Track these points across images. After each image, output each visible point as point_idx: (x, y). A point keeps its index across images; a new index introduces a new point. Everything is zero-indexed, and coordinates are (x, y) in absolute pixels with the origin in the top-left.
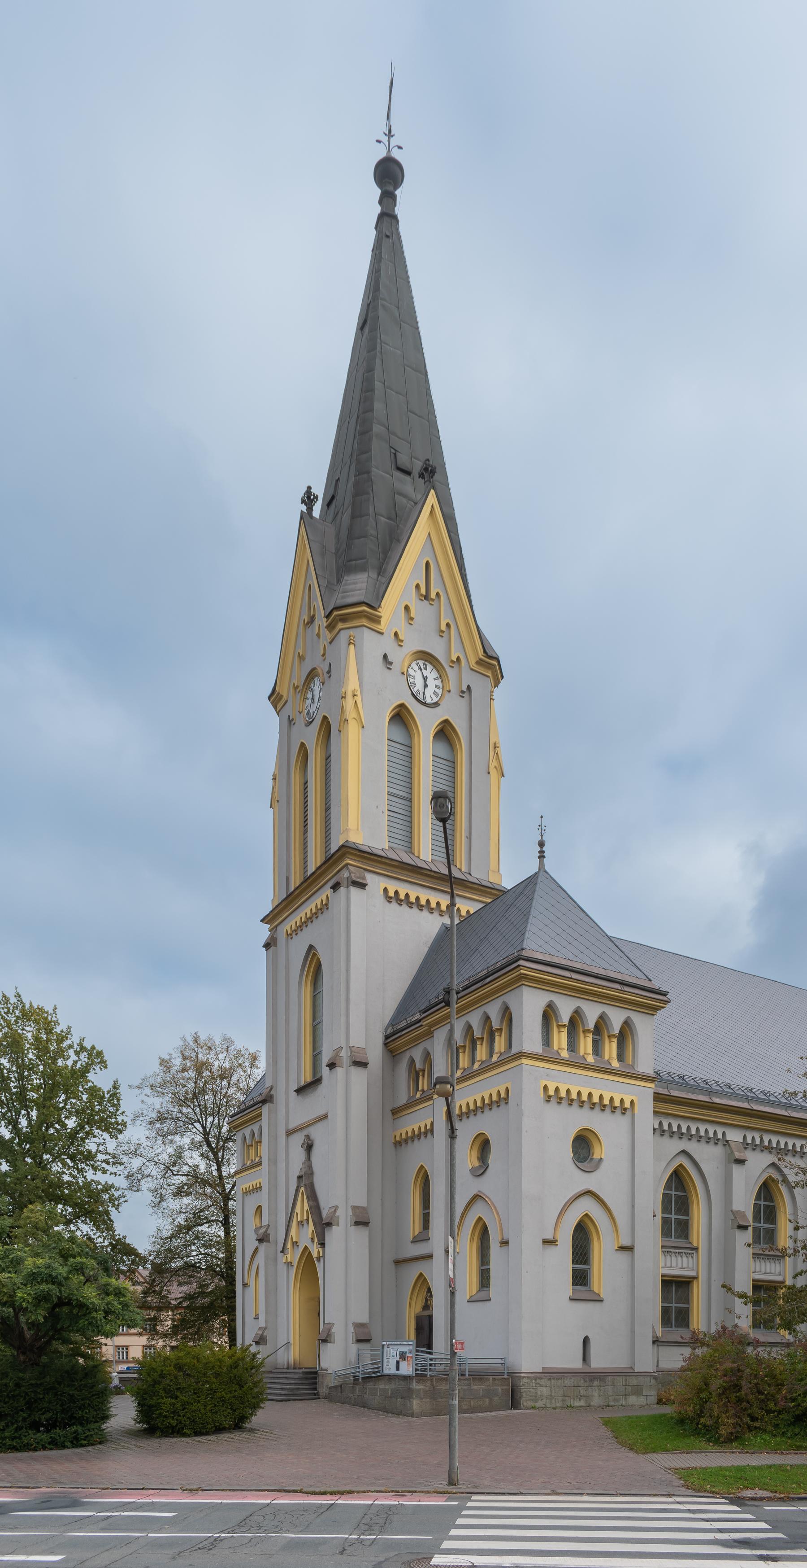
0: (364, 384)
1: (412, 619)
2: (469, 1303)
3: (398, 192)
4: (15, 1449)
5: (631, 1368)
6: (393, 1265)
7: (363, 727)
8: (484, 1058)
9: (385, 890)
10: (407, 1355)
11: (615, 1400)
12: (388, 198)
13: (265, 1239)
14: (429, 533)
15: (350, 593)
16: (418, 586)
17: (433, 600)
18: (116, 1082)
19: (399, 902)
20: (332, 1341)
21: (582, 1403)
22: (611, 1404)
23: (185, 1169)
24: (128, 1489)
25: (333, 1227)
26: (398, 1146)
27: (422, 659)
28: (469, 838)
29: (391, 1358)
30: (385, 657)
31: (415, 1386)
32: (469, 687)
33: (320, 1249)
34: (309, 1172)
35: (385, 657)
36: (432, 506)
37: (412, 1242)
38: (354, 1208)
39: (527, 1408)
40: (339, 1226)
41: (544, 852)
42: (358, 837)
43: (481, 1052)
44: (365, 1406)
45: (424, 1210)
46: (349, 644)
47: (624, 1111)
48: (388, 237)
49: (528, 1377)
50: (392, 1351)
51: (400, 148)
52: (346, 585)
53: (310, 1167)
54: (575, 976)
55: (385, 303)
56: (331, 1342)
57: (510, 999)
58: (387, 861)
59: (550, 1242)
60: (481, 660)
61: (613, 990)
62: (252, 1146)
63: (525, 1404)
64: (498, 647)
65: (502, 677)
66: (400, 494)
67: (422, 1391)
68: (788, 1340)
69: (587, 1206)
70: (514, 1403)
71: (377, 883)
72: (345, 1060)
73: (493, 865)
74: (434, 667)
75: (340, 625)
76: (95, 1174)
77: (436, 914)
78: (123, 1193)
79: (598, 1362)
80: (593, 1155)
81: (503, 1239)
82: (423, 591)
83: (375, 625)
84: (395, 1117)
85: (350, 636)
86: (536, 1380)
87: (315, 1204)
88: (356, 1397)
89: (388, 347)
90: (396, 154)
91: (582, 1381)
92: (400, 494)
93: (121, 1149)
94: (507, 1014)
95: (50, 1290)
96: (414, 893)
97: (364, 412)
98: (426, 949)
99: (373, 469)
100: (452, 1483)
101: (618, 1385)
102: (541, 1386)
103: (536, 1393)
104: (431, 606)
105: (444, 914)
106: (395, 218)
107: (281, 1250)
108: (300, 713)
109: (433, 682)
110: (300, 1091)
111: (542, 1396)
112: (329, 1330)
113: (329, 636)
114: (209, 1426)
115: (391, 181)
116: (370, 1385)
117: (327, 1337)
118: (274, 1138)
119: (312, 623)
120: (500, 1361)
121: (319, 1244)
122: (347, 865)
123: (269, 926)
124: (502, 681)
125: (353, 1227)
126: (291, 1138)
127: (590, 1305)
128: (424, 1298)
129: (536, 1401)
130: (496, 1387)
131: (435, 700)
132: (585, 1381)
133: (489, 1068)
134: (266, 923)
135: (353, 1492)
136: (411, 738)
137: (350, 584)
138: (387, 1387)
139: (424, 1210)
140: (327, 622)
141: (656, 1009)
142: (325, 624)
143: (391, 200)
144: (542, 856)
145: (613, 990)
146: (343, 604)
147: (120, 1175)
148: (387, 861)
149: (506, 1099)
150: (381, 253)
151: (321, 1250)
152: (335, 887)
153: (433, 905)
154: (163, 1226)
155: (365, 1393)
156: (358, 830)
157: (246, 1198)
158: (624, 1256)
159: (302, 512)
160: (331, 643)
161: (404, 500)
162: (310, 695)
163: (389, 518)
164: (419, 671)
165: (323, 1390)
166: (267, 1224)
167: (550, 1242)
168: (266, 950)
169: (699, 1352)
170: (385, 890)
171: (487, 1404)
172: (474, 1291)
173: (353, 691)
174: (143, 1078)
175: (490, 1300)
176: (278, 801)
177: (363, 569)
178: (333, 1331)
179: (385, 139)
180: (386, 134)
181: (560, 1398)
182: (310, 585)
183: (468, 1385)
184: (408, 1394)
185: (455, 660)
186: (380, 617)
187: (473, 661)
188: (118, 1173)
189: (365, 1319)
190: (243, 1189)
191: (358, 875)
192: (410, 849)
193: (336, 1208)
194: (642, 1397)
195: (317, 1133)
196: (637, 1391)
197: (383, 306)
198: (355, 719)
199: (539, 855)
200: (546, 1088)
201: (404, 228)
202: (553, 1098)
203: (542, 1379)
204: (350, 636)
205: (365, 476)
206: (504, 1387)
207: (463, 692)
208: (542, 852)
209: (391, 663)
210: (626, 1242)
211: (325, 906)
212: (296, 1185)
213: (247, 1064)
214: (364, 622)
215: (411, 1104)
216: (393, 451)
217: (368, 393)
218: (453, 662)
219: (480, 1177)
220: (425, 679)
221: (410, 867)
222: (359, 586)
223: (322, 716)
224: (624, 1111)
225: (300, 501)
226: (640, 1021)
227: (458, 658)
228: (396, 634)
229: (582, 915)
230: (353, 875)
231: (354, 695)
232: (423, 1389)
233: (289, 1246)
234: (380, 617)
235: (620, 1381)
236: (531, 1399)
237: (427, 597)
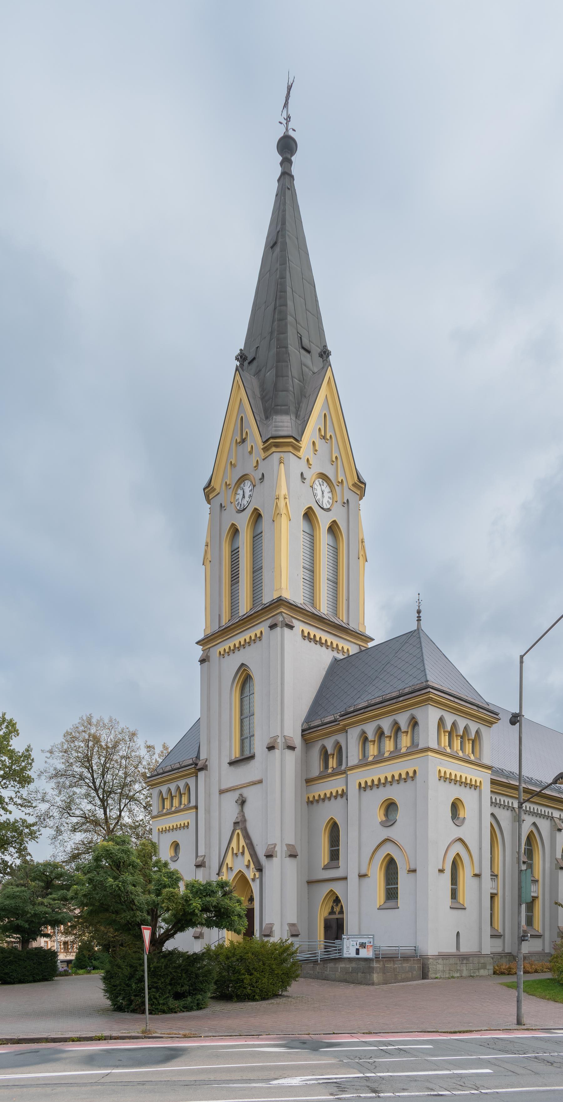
0: (279, 286)
1: (316, 451)
2: (379, 910)
3: (293, 158)
4: (164, 1012)
5: (479, 952)
6: (306, 884)
7: (290, 520)
8: (392, 749)
9: (303, 631)
10: (367, 944)
11: (474, 973)
12: (286, 162)
13: (203, 865)
14: (326, 395)
15: (281, 428)
16: (320, 429)
17: (328, 440)
18: (29, 746)
19: (310, 639)
20: (273, 936)
21: (458, 975)
22: (472, 975)
23: (78, 812)
24: (324, 1034)
25: (274, 858)
26: (310, 804)
27: (321, 478)
28: (348, 600)
29: (351, 947)
30: (302, 474)
31: (375, 965)
32: (348, 500)
33: (256, 873)
34: (243, 820)
35: (302, 474)
36: (329, 378)
38: (288, 845)
39: (432, 979)
40: (277, 857)
41: (420, 617)
42: (287, 595)
43: (389, 746)
44: (326, 979)
45: (331, 847)
46: (280, 463)
47: (476, 787)
48: (289, 189)
49: (433, 958)
50: (352, 942)
51: (294, 130)
52: (276, 422)
53: (244, 816)
54: (456, 700)
55: (289, 234)
56: (272, 937)
57: (418, 713)
58: (305, 612)
59: (441, 871)
60: (355, 483)
61: (473, 710)
62: (167, 799)
63: (431, 976)
64: (365, 477)
65: (364, 496)
66: (305, 365)
67: (378, 968)
68: (500, 932)
69: (458, 848)
70: (425, 976)
71: (299, 626)
72: (280, 744)
73: (361, 621)
74: (328, 484)
75: (274, 449)
76: (6, 814)
77: (330, 649)
78: (39, 828)
79: (464, 949)
80: (459, 815)
81: (410, 868)
82: (323, 433)
83: (297, 452)
84: (308, 785)
85: (281, 458)
86: (436, 960)
87: (250, 842)
88: (317, 973)
89: (293, 264)
90: (291, 133)
91: (458, 961)
92: (305, 365)
93: (31, 796)
94: (414, 723)
96: (320, 635)
97: (280, 306)
98: (324, 673)
99: (289, 346)
100: (519, 1022)
101: (475, 962)
102: (439, 964)
103: (436, 968)
104: (326, 444)
105: (334, 650)
106: (292, 177)
107: (217, 873)
108: (231, 503)
109: (327, 495)
110: (231, 763)
111: (439, 970)
112: (272, 928)
113: (263, 455)
114: (270, 994)
115: (289, 152)
116: (331, 965)
117: (270, 933)
118: (208, 796)
119: (242, 443)
121: (256, 869)
122: (281, 612)
123: (202, 647)
124: (364, 498)
125: (288, 859)
126: (223, 796)
127: (460, 911)
128: (331, 906)
129: (436, 974)
130: (414, 965)
131: (328, 506)
132: (460, 961)
133: (399, 756)
134: (200, 645)
135: (473, 1031)
136: (313, 530)
137: (279, 422)
138: (347, 966)
139: (331, 847)
140: (263, 445)
141: (492, 723)
142: (262, 447)
143: (289, 165)
144: (419, 620)
145: (473, 710)
146: (278, 435)
147: (33, 815)
148: (305, 612)
149: (413, 778)
150: (285, 199)
151: (257, 875)
152: (272, 627)
153: (329, 644)
154: (57, 853)
155: (326, 971)
156: (287, 589)
157: (161, 836)
158: (476, 879)
159: (237, 365)
160: (264, 460)
161: (307, 370)
162: (240, 492)
163: (300, 381)
164: (319, 486)
166: (204, 854)
167: (441, 871)
168: (200, 664)
170: (303, 631)
171: (410, 976)
172: (382, 903)
173: (285, 495)
174: (52, 745)
175: (398, 908)
176: (210, 561)
177: (287, 413)
178: (273, 929)
179: (284, 122)
180: (285, 119)
181: (448, 972)
182: (242, 417)
183: (401, 964)
184: (371, 970)
185: (340, 481)
186: (301, 447)
187: (350, 484)
188: (32, 813)
189: (294, 921)
190: (159, 829)
191: (288, 620)
192: (313, 604)
193: (275, 845)
194: (486, 970)
195: (249, 793)
196: (484, 967)
197: (288, 235)
198: (285, 514)
200: (440, 771)
201: (298, 184)
202: (444, 778)
203: (439, 959)
204: (281, 458)
205: (284, 349)
206: (419, 965)
207: (344, 503)
208: (419, 617)
209: (305, 479)
210: (477, 872)
211: (259, 638)
212: (232, 828)
213: (127, 738)
214: (291, 449)
215: (322, 777)
216: (299, 335)
217: (281, 293)
218: (339, 482)
219: (384, 828)
221: (318, 617)
222: (286, 424)
223: (253, 508)
224: (476, 787)
225: (235, 358)
226: (484, 730)
227: (342, 480)
228: (308, 460)
230: (286, 620)
231: (285, 498)
232: (379, 967)
233: (224, 869)
234: (301, 447)
235: (476, 960)
236: (433, 973)
237: (324, 437)
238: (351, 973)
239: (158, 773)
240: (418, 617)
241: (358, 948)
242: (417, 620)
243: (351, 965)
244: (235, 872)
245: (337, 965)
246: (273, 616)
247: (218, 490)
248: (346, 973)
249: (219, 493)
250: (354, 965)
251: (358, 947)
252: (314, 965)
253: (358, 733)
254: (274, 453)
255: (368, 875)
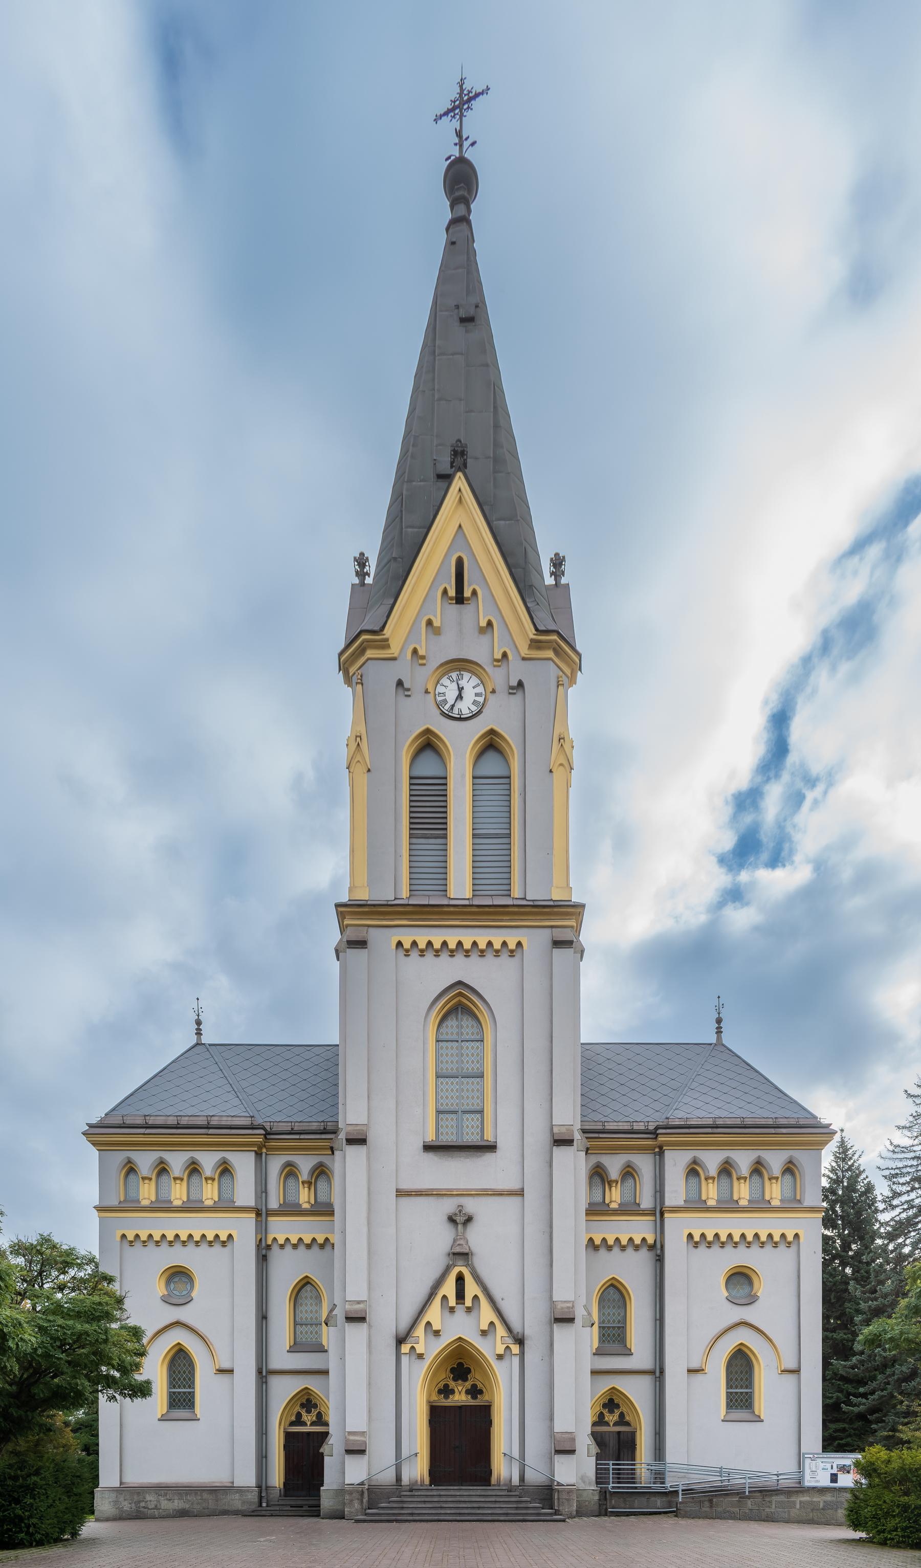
29: (820, 1472)
37: (288, 1352)
60: (532, 640)
75: (550, 654)
82: (452, 593)
95: (837, 1395)
110: (428, 1148)
120: (719, 1470)
151: (515, 1349)
165: (326, 1502)
169: (23, 1515)
172: (165, 1411)
199: (716, 1030)
220: (461, 689)
223: (489, 728)
229: (781, 1095)
233: (420, 1331)
238: (822, 1509)
239: (124, 1123)
240: (196, 1029)
241: (836, 1472)
242: (196, 1034)
243: (824, 1498)
244: (447, 1339)
245: (792, 1499)
246: (552, 927)
247: (394, 650)
248: (812, 1510)
249: (394, 659)
250: (828, 1497)
251: (835, 1471)
252: (740, 1498)
253: (752, 1160)
254: (369, 661)
255: (703, 1370)
